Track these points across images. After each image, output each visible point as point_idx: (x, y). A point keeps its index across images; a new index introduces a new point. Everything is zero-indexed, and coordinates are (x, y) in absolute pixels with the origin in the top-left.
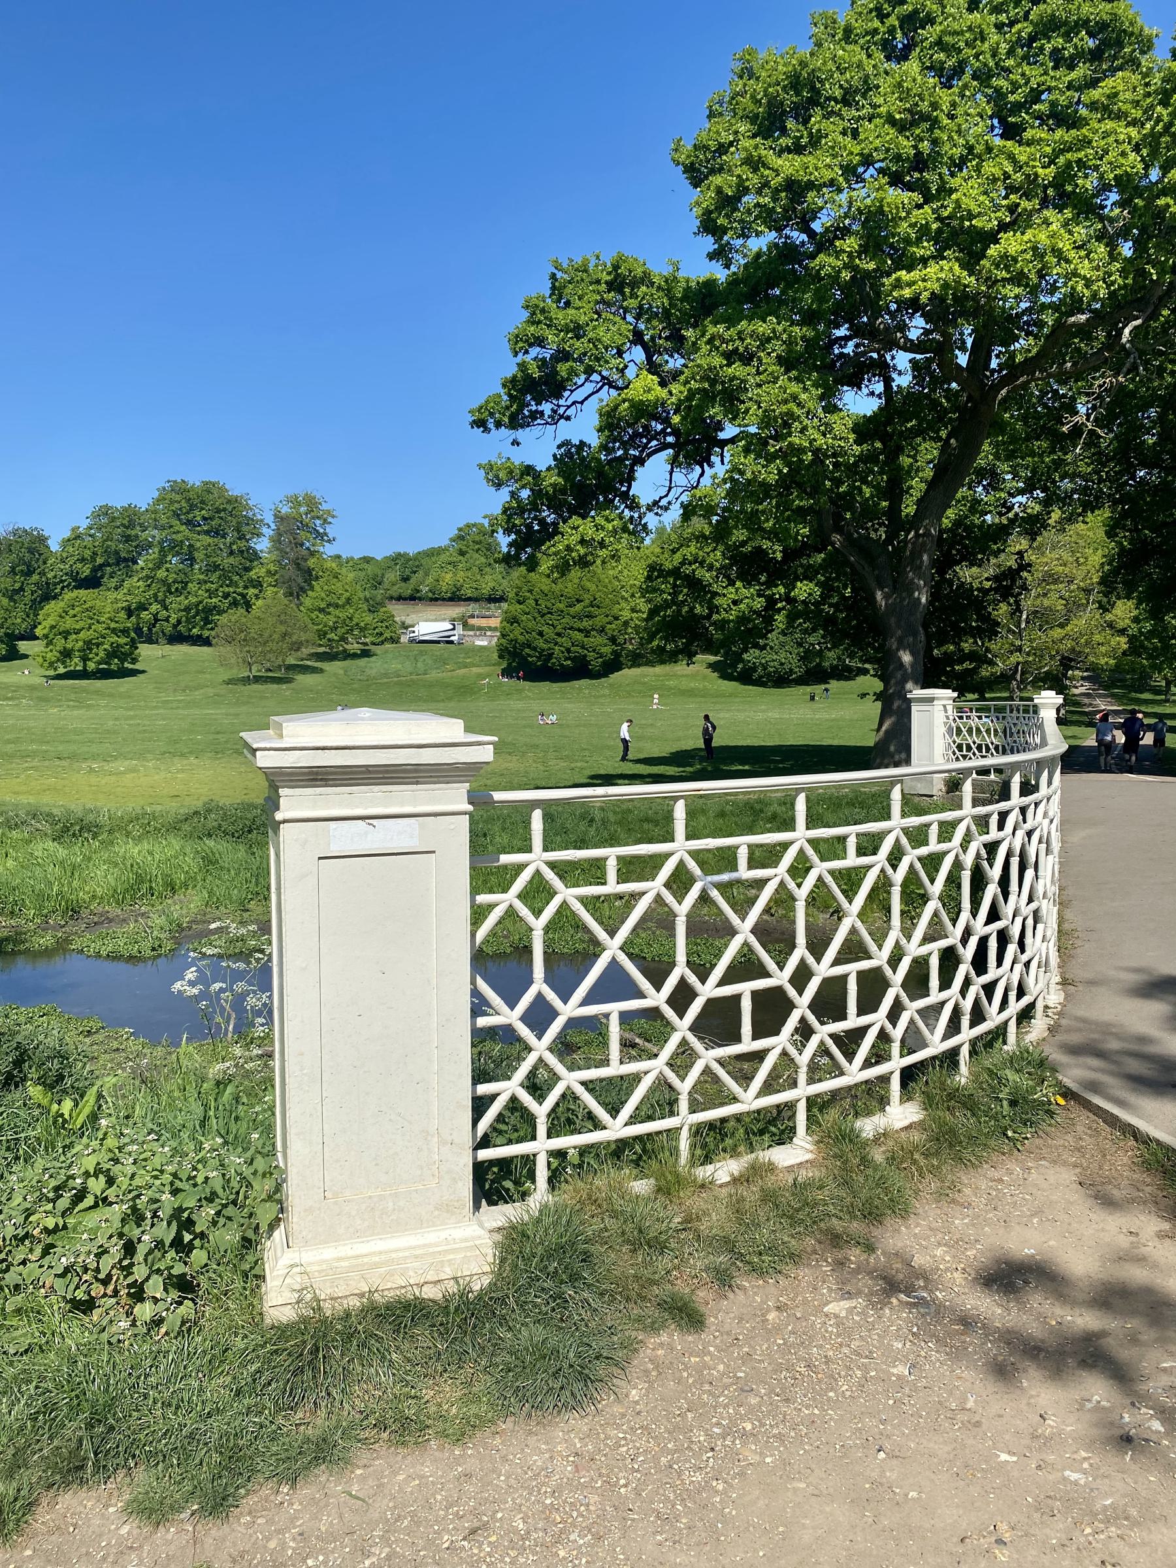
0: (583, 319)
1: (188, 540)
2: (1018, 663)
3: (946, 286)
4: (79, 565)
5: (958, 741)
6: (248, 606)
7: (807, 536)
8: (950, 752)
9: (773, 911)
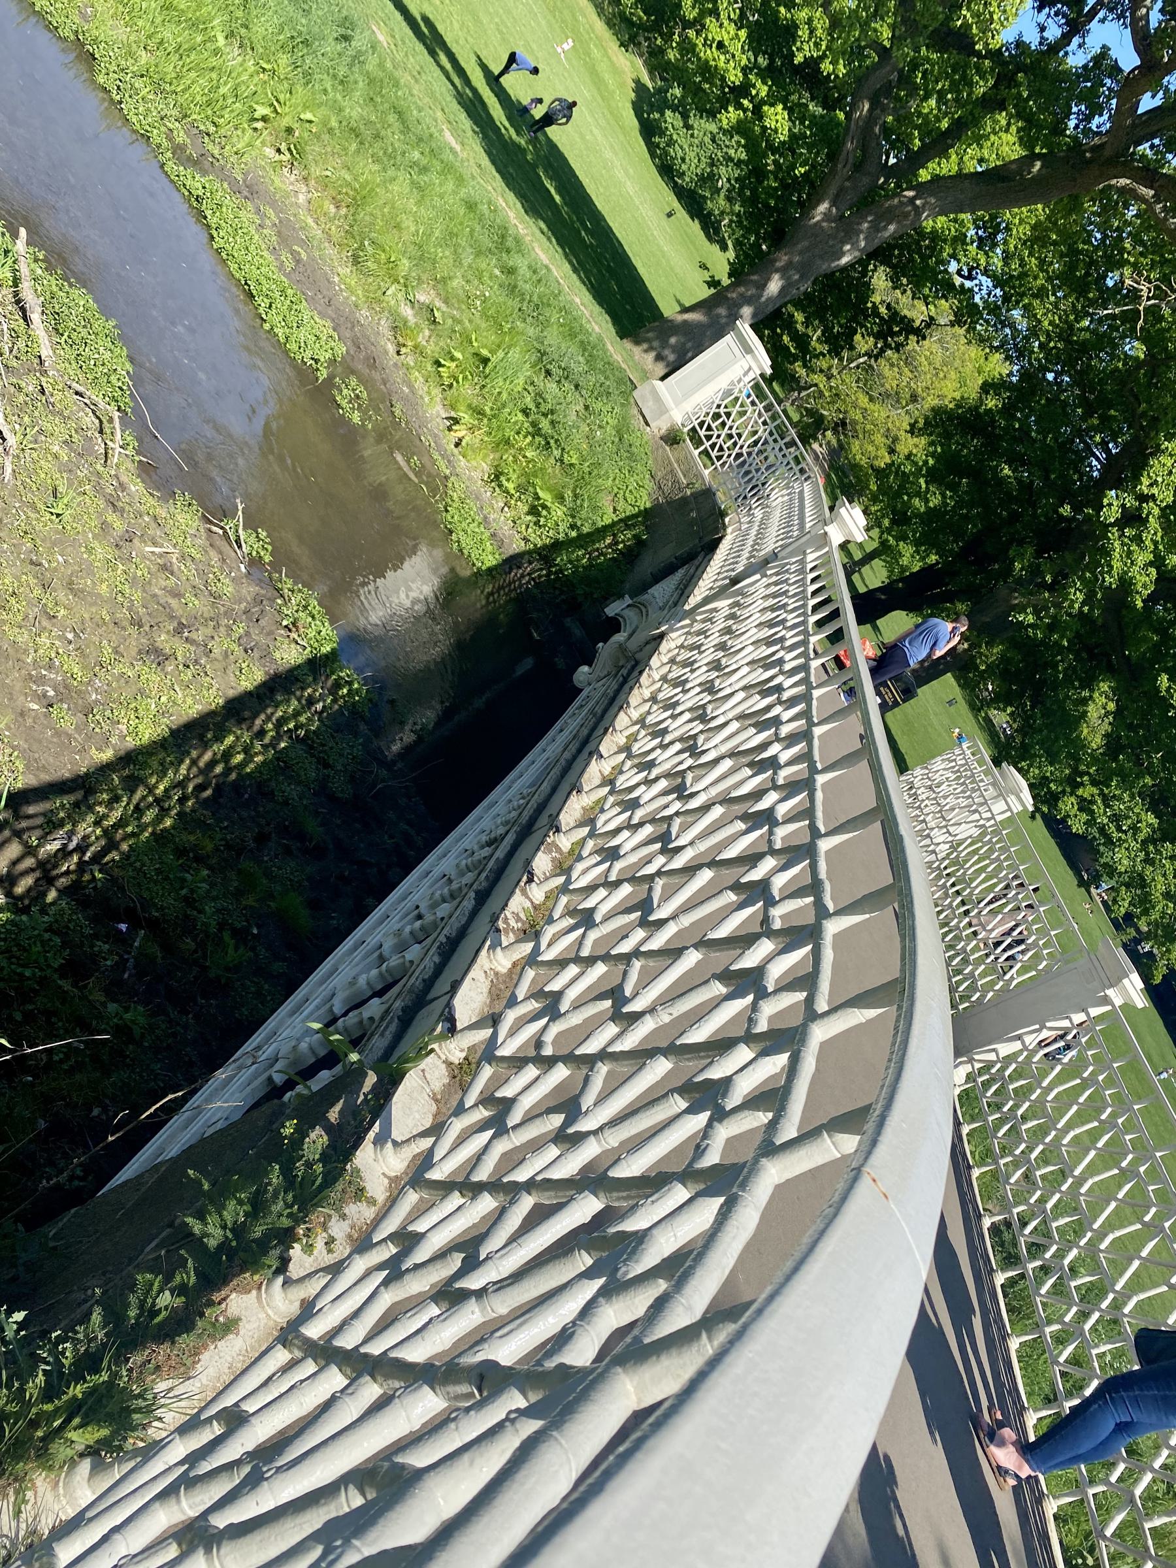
7: (837, 76)
8: (705, 410)
9: (403, 350)
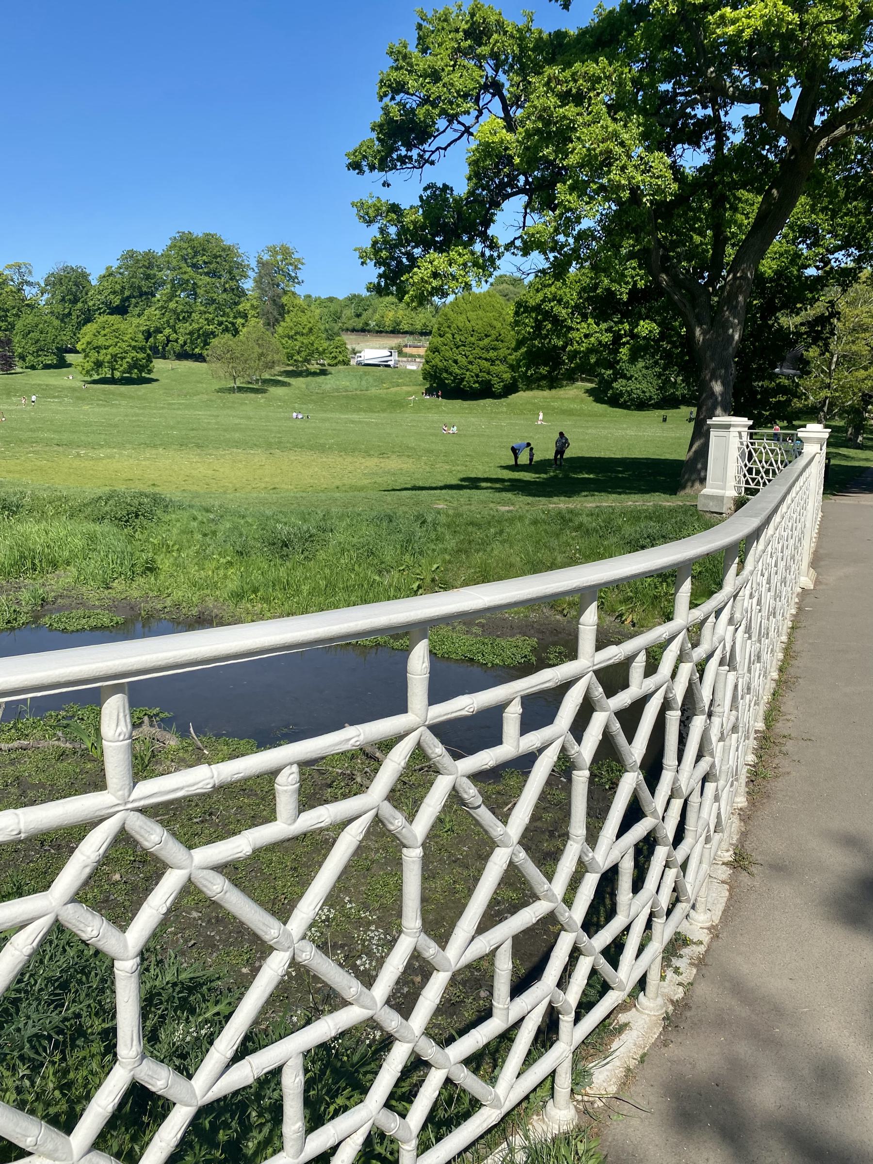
0: (440, 64)
2: (826, 398)
3: (768, 23)
4: (112, 297)
5: (749, 465)
6: (236, 332)
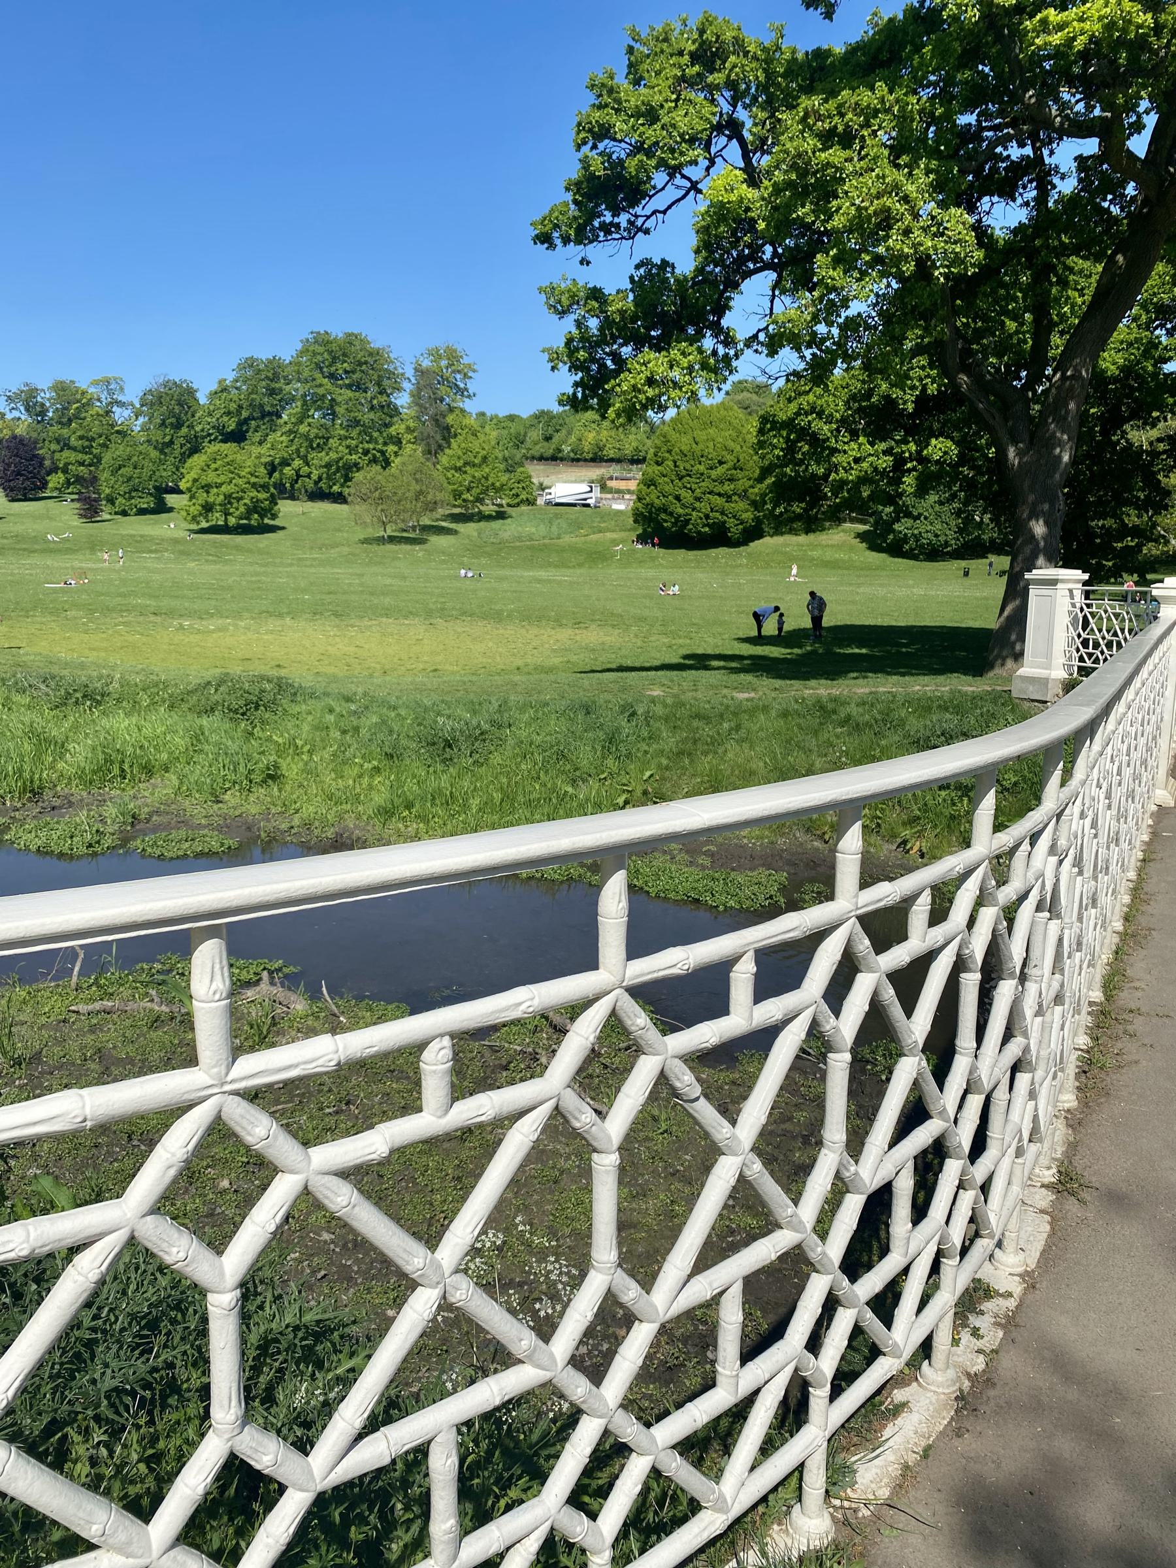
1: (330, 393)
4: (225, 419)
5: (1084, 635)
6: (387, 463)
